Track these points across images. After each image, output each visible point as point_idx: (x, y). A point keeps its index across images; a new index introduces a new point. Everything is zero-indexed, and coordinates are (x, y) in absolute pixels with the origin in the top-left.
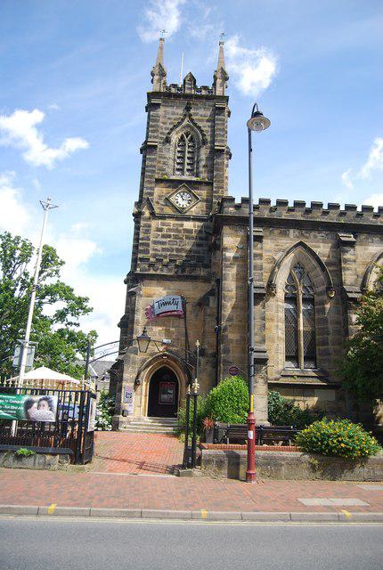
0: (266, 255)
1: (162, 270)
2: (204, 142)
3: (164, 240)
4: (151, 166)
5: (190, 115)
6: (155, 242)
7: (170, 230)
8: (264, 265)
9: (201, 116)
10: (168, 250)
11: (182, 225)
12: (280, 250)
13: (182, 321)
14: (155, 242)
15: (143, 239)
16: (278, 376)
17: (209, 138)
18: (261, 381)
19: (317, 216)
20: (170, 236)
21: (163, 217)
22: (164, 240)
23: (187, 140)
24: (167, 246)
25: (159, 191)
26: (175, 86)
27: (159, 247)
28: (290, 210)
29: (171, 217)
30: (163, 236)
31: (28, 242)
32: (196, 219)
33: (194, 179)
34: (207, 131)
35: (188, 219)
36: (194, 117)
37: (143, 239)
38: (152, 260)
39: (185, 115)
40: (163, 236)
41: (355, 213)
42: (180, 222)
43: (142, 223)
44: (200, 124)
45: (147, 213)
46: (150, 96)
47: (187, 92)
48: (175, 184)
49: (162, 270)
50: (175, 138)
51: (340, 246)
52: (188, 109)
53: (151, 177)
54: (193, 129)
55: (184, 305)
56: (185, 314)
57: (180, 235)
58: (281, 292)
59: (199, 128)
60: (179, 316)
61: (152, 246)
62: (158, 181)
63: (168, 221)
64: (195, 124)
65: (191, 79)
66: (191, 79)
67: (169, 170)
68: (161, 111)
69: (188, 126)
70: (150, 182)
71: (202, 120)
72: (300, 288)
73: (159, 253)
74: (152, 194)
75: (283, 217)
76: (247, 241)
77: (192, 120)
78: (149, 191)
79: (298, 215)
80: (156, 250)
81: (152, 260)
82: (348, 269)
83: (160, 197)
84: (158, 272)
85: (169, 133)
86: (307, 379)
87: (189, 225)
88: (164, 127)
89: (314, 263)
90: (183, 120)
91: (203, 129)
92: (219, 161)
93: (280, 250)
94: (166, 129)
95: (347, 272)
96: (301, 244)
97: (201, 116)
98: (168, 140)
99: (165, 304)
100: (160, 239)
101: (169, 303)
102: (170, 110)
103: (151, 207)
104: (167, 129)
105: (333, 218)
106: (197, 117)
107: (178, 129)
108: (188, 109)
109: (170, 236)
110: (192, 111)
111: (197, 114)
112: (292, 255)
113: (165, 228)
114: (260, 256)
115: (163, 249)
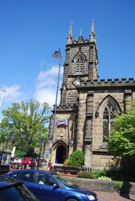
0: (94, 101)
1: (61, 109)
2: (86, 60)
3: (71, 98)
4: (67, 71)
6: (68, 99)
7: (73, 94)
8: (94, 105)
10: (72, 101)
12: (101, 99)
14: (68, 99)
15: (63, 98)
16: (99, 148)
17: (88, 59)
18: (88, 150)
19: (117, 84)
20: (73, 96)
21: (71, 89)
22: (71, 98)
23: (80, 60)
24: (72, 100)
25: (70, 79)
26: (75, 41)
27: (69, 100)
28: (106, 83)
29: (74, 89)
30: (71, 96)
31: (38, 102)
33: (83, 74)
34: (87, 56)
36: (82, 52)
37: (63, 98)
38: (67, 105)
39: (79, 51)
40: (71, 96)
41: (104, 82)
43: (63, 92)
44: (84, 54)
45: (65, 88)
46: (67, 46)
47: (80, 42)
48: (75, 77)
49: (61, 109)
50: (75, 60)
51: (126, 95)
52: (80, 49)
53: (66, 75)
56: (68, 125)
58: (101, 115)
59: (84, 55)
61: (67, 100)
62: (69, 77)
63: (72, 91)
64: (83, 54)
67: (73, 72)
68: (70, 51)
69: (80, 55)
70: (66, 77)
71: (85, 52)
72: (110, 113)
73: (69, 103)
74: (67, 81)
75: (103, 86)
76: (89, 95)
77: (81, 53)
78: (65, 80)
79: (109, 84)
80: (68, 102)
81: (67, 105)
82: (128, 104)
83: (70, 82)
84: (60, 110)
85: (73, 59)
86: (103, 149)
88: (71, 57)
89: (115, 103)
90: (78, 53)
91: (86, 55)
92: (91, 66)
93: (101, 99)
94: (72, 57)
95: (128, 106)
96: (109, 95)
98: (73, 61)
99: (61, 121)
100: (70, 98)
102: (74, 50)
103: (66, 86)
104: (72, 57)
105: (124, 84)
106: (83, 51)
107: (76, 57)
108: (80, 49)
109: (73, 96)
110: (81, 49)
111: (83, 50)
112: (106, 100)
113: (71, 93)
114: (92, 102)
115: (71, 101)
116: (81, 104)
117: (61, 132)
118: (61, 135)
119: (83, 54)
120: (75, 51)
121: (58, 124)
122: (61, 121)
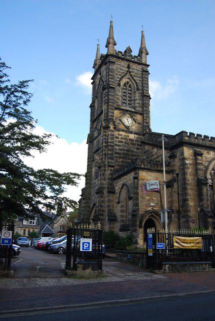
5: (130, 72)
7: (122, 138)
9: (135, 73)
10: (122, 150)
11: (128, 136)
13: (159, 194)
15: (110, 142)
20: (122, 142)
22: (119, 144)
29: (123, 131)
32: (135, 133)
35: (131, 133)
36: (132, 74)
37: (110, 142)
40: (119, 142)
42: (127, 134)
44: (135, 78)
54: (131, 81)
55: (160, 184)
57: (128, 141)
59: (135, 80)
60: (157, 191)
62: (116, 109)
63: (121, 133)
64: (133, 78)
65: (129, 50)
66: (129, 50)
85: (119, 81)
87: (132, 136)
90: (126, 74)
97: (135, 73)
98: (119, 85)
101: (154, 184)
108: (129, 67)
109: (122, 142)
116: (186, 164)
117: (151, 200)
118: (152, 204)
119: (133, 78)
120: (121, 69)
121: (148, 188)
122: (152, 185)
